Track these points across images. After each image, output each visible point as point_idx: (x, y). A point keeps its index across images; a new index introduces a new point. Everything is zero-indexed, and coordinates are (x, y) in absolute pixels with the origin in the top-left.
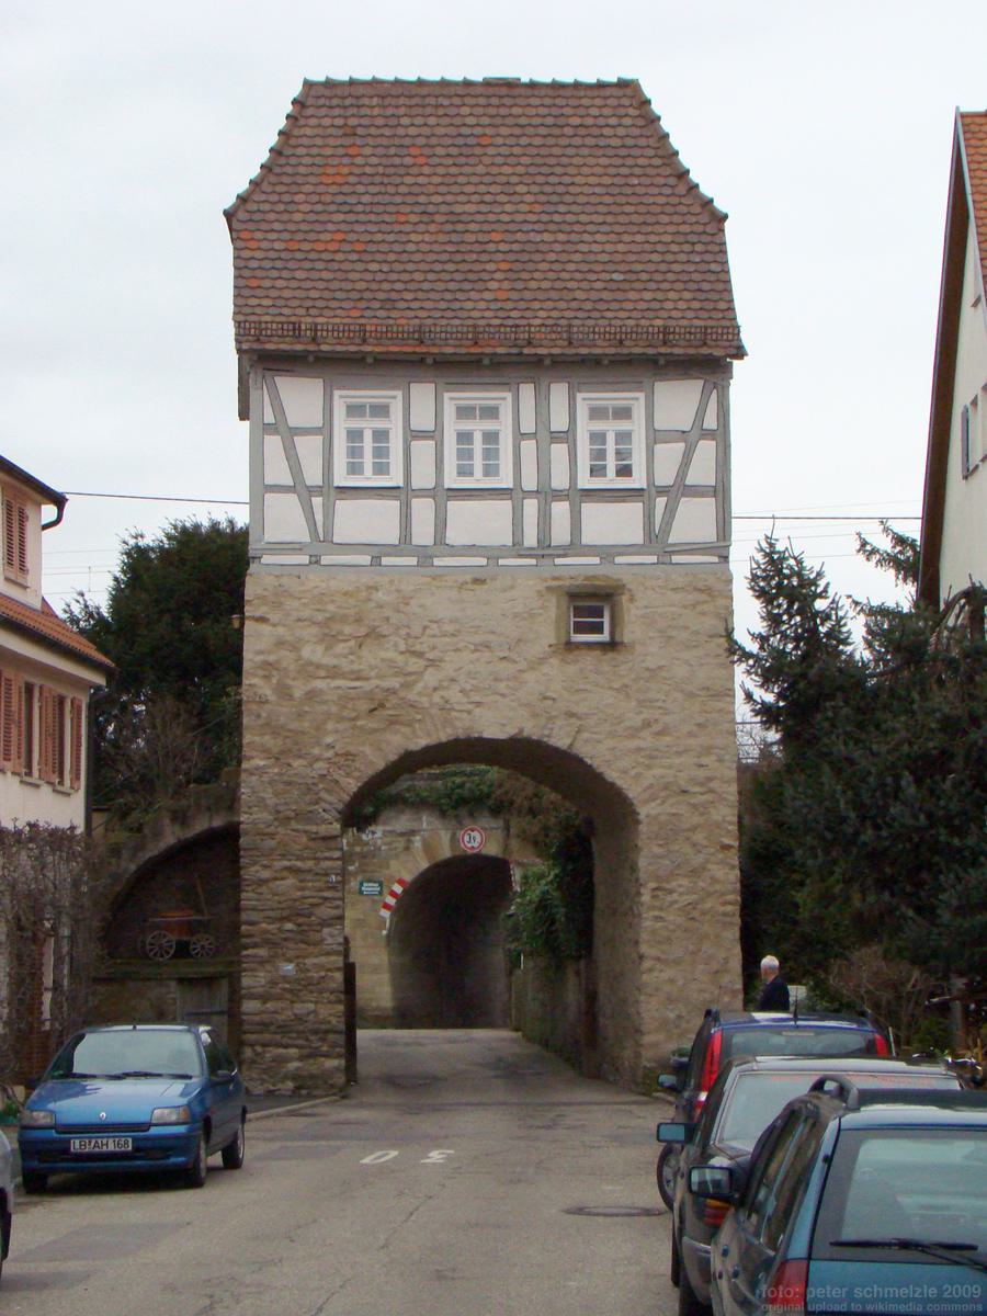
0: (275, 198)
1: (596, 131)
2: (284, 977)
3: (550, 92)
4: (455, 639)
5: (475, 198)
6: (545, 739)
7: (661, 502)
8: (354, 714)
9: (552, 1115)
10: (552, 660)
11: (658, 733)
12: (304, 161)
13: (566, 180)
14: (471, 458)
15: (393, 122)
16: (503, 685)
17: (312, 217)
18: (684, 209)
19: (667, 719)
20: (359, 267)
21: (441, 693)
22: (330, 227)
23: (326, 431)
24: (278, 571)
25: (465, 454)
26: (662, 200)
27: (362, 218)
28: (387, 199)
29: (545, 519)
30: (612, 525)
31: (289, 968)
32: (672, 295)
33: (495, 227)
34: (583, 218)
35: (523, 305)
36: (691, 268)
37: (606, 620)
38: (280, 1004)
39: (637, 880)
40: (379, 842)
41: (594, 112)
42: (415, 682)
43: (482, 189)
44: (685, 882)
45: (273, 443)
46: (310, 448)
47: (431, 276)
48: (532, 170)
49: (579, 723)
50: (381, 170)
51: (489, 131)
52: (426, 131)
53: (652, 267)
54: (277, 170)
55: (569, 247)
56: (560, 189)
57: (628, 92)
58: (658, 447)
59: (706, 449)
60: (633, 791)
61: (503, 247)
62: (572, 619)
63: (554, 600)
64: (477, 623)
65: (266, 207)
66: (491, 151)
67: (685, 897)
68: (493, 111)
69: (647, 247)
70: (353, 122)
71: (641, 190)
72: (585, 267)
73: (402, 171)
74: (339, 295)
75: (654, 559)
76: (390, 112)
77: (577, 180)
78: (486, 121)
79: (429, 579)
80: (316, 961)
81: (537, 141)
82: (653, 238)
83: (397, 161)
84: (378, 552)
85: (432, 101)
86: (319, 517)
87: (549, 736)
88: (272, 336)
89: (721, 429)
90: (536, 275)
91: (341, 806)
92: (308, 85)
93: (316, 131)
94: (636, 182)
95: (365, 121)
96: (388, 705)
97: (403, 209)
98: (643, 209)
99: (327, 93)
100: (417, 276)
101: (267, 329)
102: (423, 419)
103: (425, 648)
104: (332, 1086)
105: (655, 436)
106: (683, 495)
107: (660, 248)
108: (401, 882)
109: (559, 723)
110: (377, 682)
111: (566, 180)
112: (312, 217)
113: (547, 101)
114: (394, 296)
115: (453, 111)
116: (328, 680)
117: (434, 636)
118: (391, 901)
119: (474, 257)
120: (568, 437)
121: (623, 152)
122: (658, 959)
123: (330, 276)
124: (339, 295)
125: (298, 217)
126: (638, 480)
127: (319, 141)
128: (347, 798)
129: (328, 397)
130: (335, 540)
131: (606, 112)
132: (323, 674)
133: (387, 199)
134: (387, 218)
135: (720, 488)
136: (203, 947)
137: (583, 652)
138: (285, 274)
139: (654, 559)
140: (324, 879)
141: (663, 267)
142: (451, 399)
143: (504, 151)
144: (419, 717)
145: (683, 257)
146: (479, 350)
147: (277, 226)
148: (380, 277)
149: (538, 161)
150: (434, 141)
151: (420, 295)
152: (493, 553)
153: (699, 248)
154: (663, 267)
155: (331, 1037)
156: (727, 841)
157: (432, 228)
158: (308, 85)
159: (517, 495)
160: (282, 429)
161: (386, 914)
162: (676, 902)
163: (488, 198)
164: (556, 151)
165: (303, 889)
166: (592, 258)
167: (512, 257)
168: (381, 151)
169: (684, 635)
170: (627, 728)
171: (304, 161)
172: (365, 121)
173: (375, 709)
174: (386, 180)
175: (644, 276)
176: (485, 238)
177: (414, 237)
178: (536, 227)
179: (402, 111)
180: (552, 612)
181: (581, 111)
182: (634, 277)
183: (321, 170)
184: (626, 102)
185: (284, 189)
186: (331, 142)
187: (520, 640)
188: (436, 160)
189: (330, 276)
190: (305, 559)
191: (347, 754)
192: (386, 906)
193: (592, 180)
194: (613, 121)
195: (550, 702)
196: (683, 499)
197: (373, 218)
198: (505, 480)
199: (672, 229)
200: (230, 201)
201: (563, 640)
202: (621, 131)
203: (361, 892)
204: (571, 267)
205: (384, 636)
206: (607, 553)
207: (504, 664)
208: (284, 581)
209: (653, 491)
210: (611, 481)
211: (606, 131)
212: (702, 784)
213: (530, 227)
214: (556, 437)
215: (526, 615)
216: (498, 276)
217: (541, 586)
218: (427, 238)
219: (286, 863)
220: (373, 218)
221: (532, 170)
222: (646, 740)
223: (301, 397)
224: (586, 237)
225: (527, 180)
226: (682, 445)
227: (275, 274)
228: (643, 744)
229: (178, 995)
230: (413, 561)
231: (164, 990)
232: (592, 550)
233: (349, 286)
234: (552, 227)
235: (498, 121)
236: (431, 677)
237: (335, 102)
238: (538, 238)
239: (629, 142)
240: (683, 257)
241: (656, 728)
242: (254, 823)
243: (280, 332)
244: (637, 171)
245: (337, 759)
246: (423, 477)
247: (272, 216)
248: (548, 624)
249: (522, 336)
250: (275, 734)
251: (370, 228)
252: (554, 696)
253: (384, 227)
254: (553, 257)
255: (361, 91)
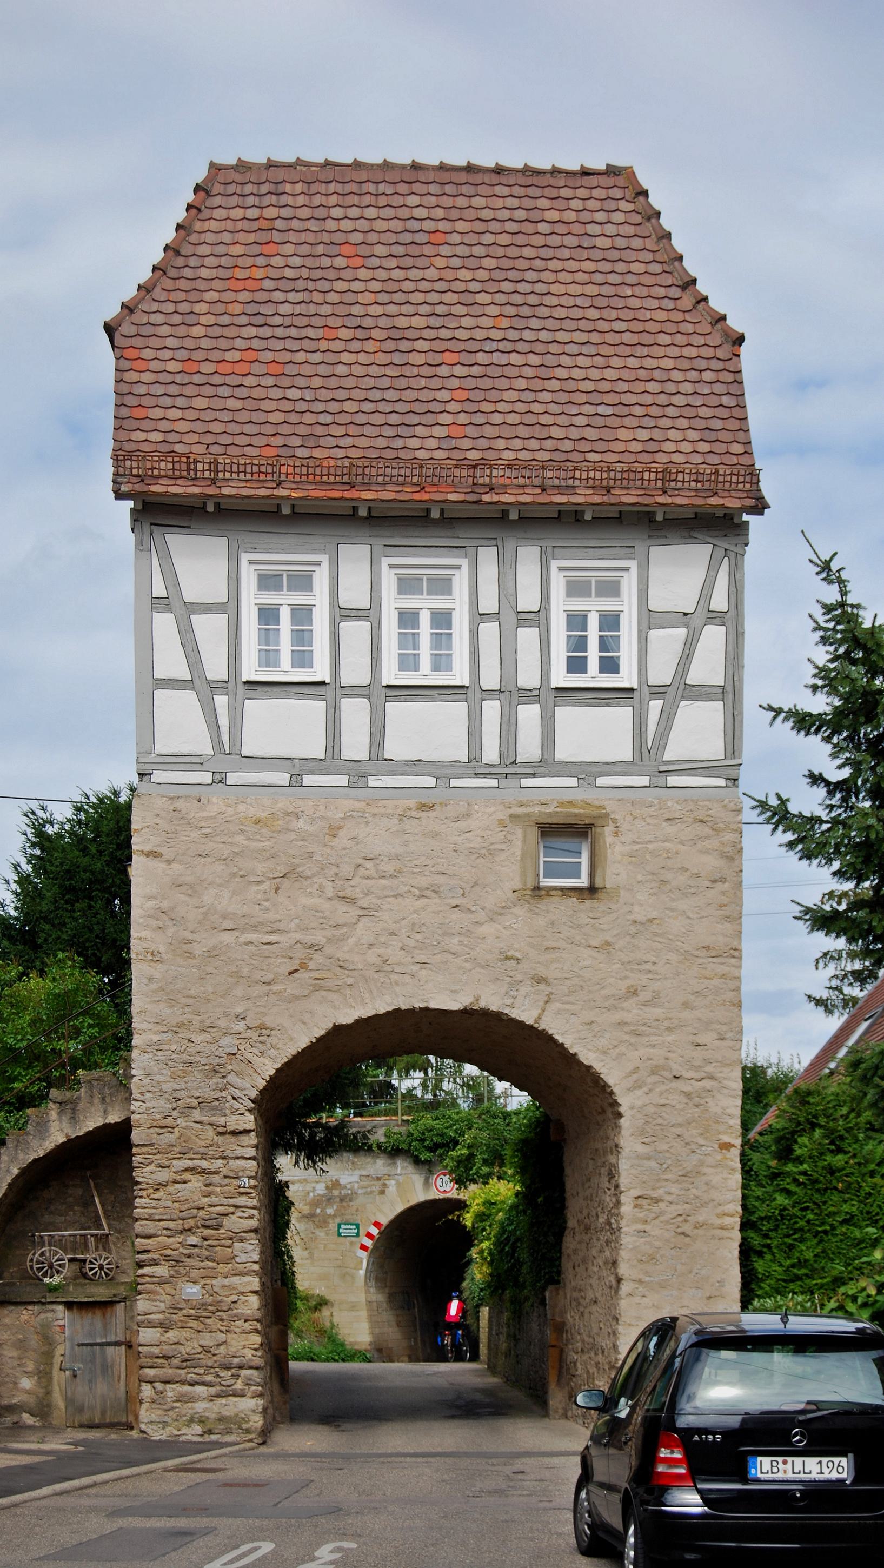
0: (170, 307)
1: (577, 228)
2: (187, 1301)
3: (522, 180)
4: (396, 882)
5: (425, 309)
6: (506, 1011)
7: (656, 706)
8: (270, 977)
9: (508, 1470)
10: (516, 910)
11: (646, 1004)
12: (207, 262)
13: (540, 288)
14: (416, 646)
15: (321, 213)
16: (455, 940)
17: (217, 331)
18: (689, 328)
19: (657, 985)
20: (276, 393)
21: (381, 951)
22: (239, 343)
23: (230, 607)
24: (173, 791)
25: (409, 640)
26: (661, 315)
27: (280, 332)
28: (312, 309)
29: (509, 727)
30: (593, 734)
31: (192, 1291)
32: (672, 434)
33: (448, 345)
34: (561, 336)
35: (483, 443)
36: (698, 401)
37: (584, 860)
38: (186, 1333)
39: (617, 1187)
40: (356, 1186)
41: (575, 204)
42: (344, 938)
43: (433, 297)
44: (675, 1189)
45: (165, 623)
46: (211, 629)
47: (367, 407)
48: (498, 275)
49: (549, 989)
50: (305, 273)
51: (442, 226)
52: (363, 225)
53: (648, 399)
54: (172, 273)
55: (543, 372)
56: (532, 299)
57: (621, 181)
58: (654, 634)
59: (714, 636)
60: (612, 1076)
61: (459, 371)
62: (542, 859)
63: (519, 832)
64: (422, 860)
65: (159, 319)
66: (445, 250)
67: (673, 1207)
68: (447, 202)
69: (642, 374)
70: (271, 212)
71: (635, 303)
72: (563, 398)
73: (331, 274)
74: (248, 429)
75: (645, 781)
76: (317, 200)
77: (554, 288)
78: (440, 213)
79: (362, 805)
80: (226, 1282)
81: (504, 239)
82: (649, 363)
83: (326, 262)
84: (298, 768)
85: (371, 188)
86: (224, 722)
87: (511, 1006)
88: (160, 477)
89: (732, 612)
90: (501, 407)
91: (254, 1094)
92: (215, 168)
93: (223, 225)
94: (629, 293)
95: (285, 212)
96: (312, 965)
97: (331, 322)
98: (638, 326)
99: (238, 178)
100: (348, 406)
101: (152, 469)
102: (355, 593)
103: (357, 892)
104: (248, 1431)
105: (650, 619)
106: (684, 698)
107: (657, 374)
108: (377, 1224)
109: (524, 990)
110: (298, 936)
111: (540, 288)
112: (217, 331)
113: (517, 191)
114: (319, 430)
115: (398, 200)
116: (236, 933)
117: (369, 878)
118: (369, 1243)
119: (423, 383)
120: (537, 618)
121: (615, 255)
122: (640, 1282)
123: (238, 404)
124: (248, 429)
125: (197, 331)
126: (627, 677)
127: (227, 238)
128: (262, 1084)
129: (234, 563)
130: (245, 752)
131: (591, 204)
132: (228, 924)
133: (312, 309)
134: (311, 333)
135: (729, 688)
136: (101, 1267)
137: (556, 900)
138: (180, 402)
139: (645, 781)
140: (236, 1182)
141: (663, 399)
142: (392, 567)
143: (461, 250)
144: (350, 981)
145: (688, 388)
146: (425, 497)
147: (171, 342)
148: (302, 406)
149: (506, 263)
150: (373, 238)
151: (352, 430)
152: (443, 771)
153: (708, 376)
154: (663, 399)
155: (244, 1373)
156: (726, 1139)
157: (370, 346)
158: (215, 168)
159: (474, 695)
160: (176, 603)
161: (364, 1255)
162: (662, 1213)
163: (440, 309)
164: (527, 252)
165: (208, 1195)
166: (571, 386)
167: (471, 383)
168: (305, 249)
169: (682, 879)
170: (608, 997)
171: (207, 262)
172: (285, 212)
173: (296, 971)
174: (311, 285)
175: (638, 411)
176: (438, 358)
177: (346, 357)
178: (501, 346)
179: (333, 200)
180: (517, 848)
181: (560, 204)
182: (625, 411)
183: (228, 273)
184: (617, 193)
185: (182, 296)
186: (242, 237)
187: (476, 884)
188: (375, 262)
189: (238, 404)
190: (207, 778)
191: (262, 1027)
192: (364, 1247)
193: (573, 289)
194: (600, 217)
195: (513, 963)
196: (683, 703)
197: (293, 332)
198: (460, 675)
199: (674, 351)
200: (112, 311)
201: (530, 884)
202: (610, 229)
203: (339, 1235)
204: (546, 397)
205: (306, 878)
206: (587, 771)
207: (456, 915)
208: (180, 804)
209: (646, 690)
210: (593, 677)
211: (591, 229)
212: (697, 1068)
213: (494, 346)
214: (525, 619)
215: (483, 851)
216: (453, 407)
217: (503, 814)
218: (362, 358)
219: (190, 1164)
220: (293, 332)
221: (498, 275)
222: (632, 1011)
223: (200, 562)
224: (565, 360)
225: (493, 287)
226: (683, 631)
227: (167, 401)
228: (628, 1017)
229: (66, 1322)
230: (343, 780)
231: (49, 1315)
232: (567, 768)
233: (261, 417)
234: (521, 347)
235: (455, 214)
236: (364, 932)
237: (248, 189)
238: (504, 359)
239: (620, 242)
240: (688, 388)
241: (644, 996)
242: (147, 1112)
243: (171, 473)
244: (630, 279)
245: (250, 1034)
246: (355, 671)
247: (165, 330)
248: (514, 858)
249: (481, 481)
250: (172, 1002)
251: (289, 344)
252: (518, 955)
253: (307, 344)
254: (522, 384)
255: (280, 175)
